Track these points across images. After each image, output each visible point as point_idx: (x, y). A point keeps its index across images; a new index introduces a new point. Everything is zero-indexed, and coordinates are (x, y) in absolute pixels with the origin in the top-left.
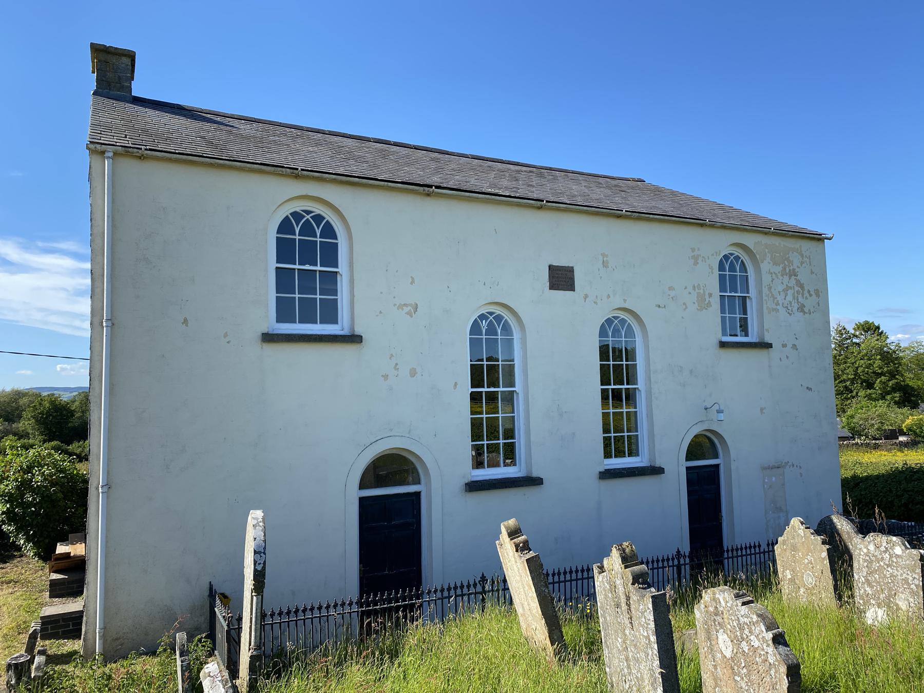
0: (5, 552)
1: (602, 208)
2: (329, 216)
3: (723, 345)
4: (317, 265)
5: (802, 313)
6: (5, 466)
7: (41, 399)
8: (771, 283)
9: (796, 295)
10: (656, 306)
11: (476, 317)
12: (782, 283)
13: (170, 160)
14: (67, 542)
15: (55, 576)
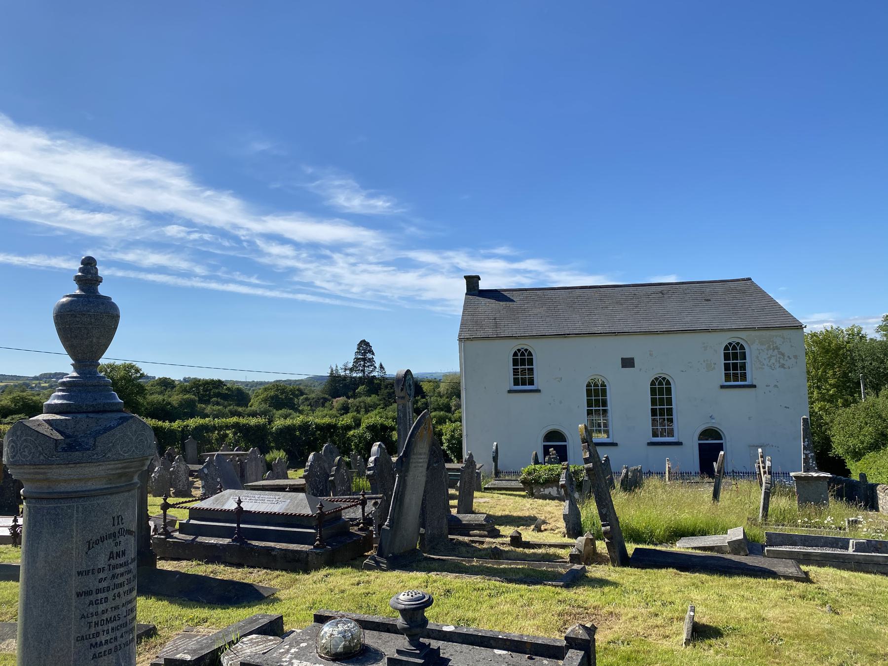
9: (778, 359)
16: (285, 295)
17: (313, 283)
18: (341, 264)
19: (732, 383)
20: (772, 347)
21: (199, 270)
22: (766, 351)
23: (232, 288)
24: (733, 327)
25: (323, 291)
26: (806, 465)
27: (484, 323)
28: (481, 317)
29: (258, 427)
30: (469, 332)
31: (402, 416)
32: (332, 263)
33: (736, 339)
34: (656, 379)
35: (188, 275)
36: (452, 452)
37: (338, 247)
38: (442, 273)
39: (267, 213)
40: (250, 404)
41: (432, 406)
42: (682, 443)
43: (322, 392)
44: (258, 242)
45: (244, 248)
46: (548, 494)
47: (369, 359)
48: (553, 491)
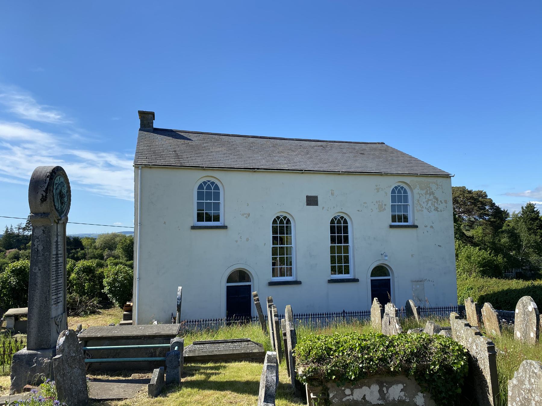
0: (109, 305)
1: (331, 171)
2: (217, 182)
3: (391, 227)
4: (212, 200)
5: (436, 211)
6: (108, 272)
7: (126, 239)
8: (419, 198)
9: (433, 203)
10: (357, 211)
12: (426, 198)
13: (160, 168)
14: (130, 302)
15: (125, 313)
19: (397, 224)
20: (429, 192)
25: (5, 173)
30: (147, 160)
31: (40, 248)
32: (12, 153)
36: (114, 296)
37: (17, 142)
38: (98, 167)
41: (89, 256)
46: (360, 399)
48: (372, 392)
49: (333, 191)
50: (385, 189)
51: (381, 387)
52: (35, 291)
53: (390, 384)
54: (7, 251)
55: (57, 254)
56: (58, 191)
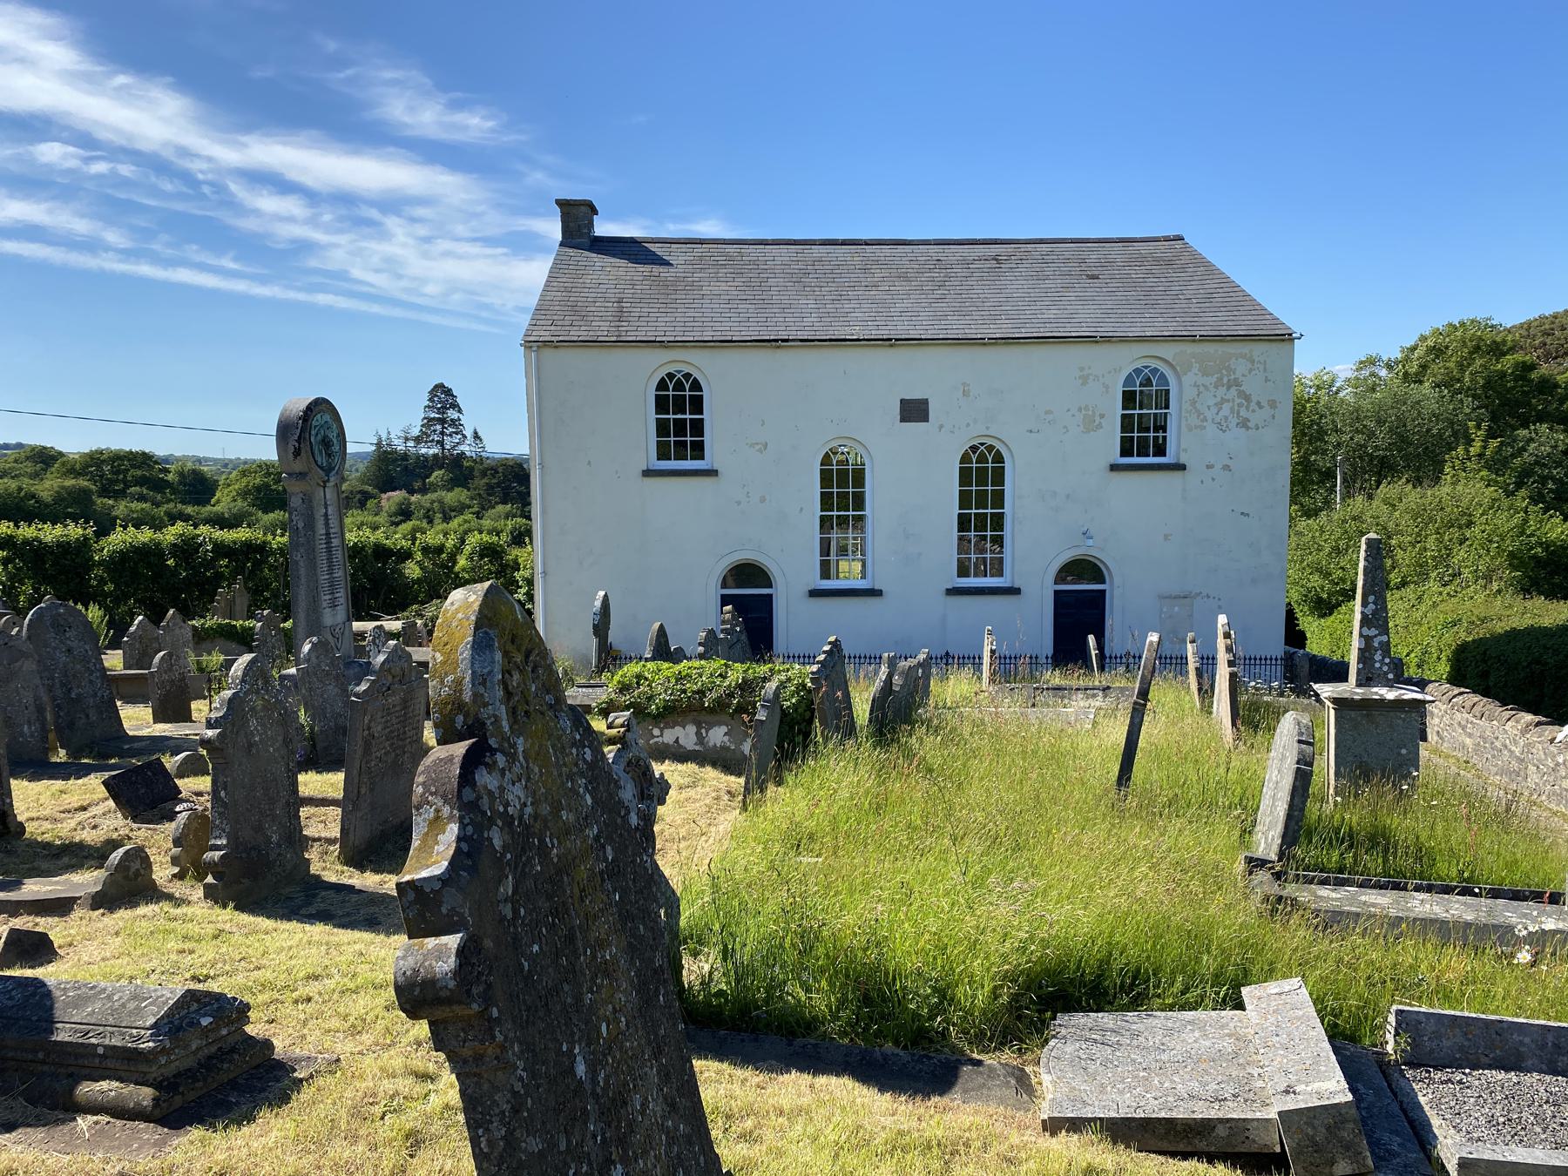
9: (1236, 408)
11: (967, 447)
12: (1215, 396)
16: (292, 295)
17: (346, 272)
18: (401, 238)
19: (1136, 460)
21: (112, 237)
22: (1213, 390)
23: (183, 275)
24: (1148, 334)
25: (365, 289)
26: (1364, 668)
27: (593, 309)
28: (587, 295)
29: (63, 547)
31: (300, 525)
32: (384, 235)
33: (1153, 361)
34: (974, 448)
35: (91, 245)
37: (393, 204)
39: (249, 128)
40: (213, 501)
42: (1019, 589)
43: (362, 481)
44: (233, 187)
45: (203, 197)
46: (671, 743)
47: (452, 420)
48: (687, 734)
49: (969, 385)
50: (1103, 376)
51: (699, 727)
52: (298, 586)
53: (710, 726)
54: (384, 496)
55: (328, 534)
56: (319, 437)
